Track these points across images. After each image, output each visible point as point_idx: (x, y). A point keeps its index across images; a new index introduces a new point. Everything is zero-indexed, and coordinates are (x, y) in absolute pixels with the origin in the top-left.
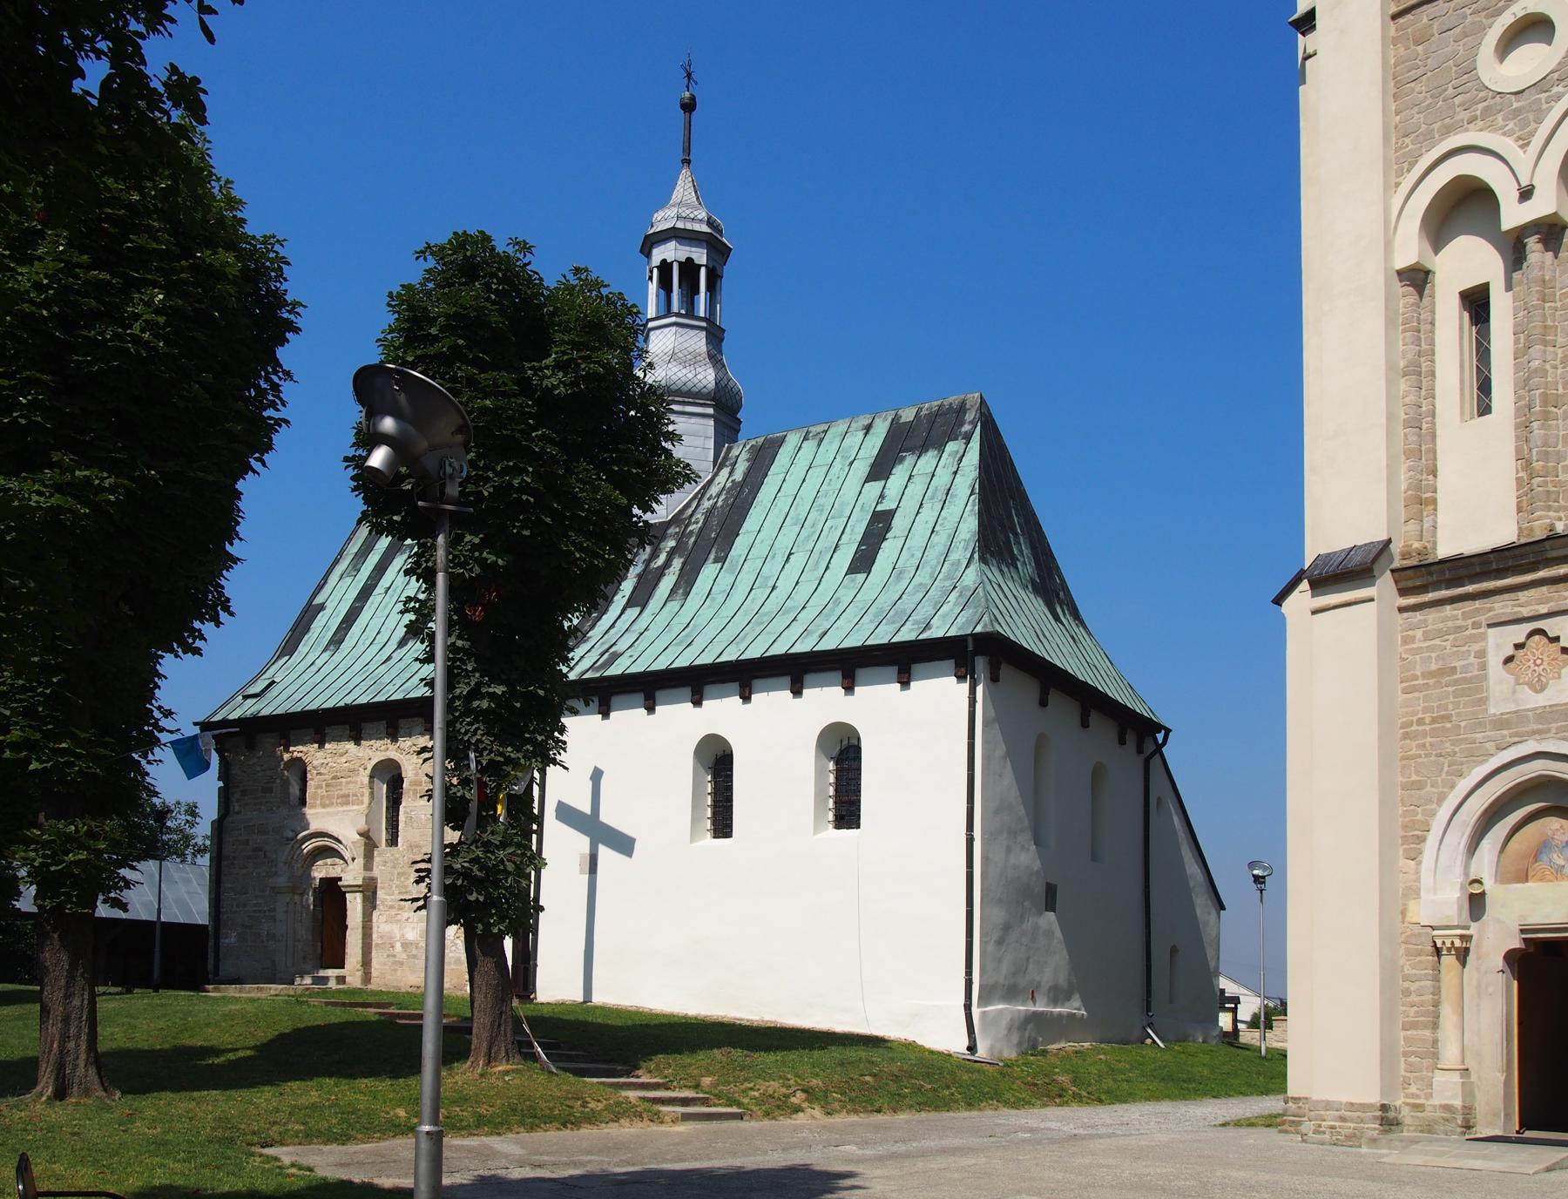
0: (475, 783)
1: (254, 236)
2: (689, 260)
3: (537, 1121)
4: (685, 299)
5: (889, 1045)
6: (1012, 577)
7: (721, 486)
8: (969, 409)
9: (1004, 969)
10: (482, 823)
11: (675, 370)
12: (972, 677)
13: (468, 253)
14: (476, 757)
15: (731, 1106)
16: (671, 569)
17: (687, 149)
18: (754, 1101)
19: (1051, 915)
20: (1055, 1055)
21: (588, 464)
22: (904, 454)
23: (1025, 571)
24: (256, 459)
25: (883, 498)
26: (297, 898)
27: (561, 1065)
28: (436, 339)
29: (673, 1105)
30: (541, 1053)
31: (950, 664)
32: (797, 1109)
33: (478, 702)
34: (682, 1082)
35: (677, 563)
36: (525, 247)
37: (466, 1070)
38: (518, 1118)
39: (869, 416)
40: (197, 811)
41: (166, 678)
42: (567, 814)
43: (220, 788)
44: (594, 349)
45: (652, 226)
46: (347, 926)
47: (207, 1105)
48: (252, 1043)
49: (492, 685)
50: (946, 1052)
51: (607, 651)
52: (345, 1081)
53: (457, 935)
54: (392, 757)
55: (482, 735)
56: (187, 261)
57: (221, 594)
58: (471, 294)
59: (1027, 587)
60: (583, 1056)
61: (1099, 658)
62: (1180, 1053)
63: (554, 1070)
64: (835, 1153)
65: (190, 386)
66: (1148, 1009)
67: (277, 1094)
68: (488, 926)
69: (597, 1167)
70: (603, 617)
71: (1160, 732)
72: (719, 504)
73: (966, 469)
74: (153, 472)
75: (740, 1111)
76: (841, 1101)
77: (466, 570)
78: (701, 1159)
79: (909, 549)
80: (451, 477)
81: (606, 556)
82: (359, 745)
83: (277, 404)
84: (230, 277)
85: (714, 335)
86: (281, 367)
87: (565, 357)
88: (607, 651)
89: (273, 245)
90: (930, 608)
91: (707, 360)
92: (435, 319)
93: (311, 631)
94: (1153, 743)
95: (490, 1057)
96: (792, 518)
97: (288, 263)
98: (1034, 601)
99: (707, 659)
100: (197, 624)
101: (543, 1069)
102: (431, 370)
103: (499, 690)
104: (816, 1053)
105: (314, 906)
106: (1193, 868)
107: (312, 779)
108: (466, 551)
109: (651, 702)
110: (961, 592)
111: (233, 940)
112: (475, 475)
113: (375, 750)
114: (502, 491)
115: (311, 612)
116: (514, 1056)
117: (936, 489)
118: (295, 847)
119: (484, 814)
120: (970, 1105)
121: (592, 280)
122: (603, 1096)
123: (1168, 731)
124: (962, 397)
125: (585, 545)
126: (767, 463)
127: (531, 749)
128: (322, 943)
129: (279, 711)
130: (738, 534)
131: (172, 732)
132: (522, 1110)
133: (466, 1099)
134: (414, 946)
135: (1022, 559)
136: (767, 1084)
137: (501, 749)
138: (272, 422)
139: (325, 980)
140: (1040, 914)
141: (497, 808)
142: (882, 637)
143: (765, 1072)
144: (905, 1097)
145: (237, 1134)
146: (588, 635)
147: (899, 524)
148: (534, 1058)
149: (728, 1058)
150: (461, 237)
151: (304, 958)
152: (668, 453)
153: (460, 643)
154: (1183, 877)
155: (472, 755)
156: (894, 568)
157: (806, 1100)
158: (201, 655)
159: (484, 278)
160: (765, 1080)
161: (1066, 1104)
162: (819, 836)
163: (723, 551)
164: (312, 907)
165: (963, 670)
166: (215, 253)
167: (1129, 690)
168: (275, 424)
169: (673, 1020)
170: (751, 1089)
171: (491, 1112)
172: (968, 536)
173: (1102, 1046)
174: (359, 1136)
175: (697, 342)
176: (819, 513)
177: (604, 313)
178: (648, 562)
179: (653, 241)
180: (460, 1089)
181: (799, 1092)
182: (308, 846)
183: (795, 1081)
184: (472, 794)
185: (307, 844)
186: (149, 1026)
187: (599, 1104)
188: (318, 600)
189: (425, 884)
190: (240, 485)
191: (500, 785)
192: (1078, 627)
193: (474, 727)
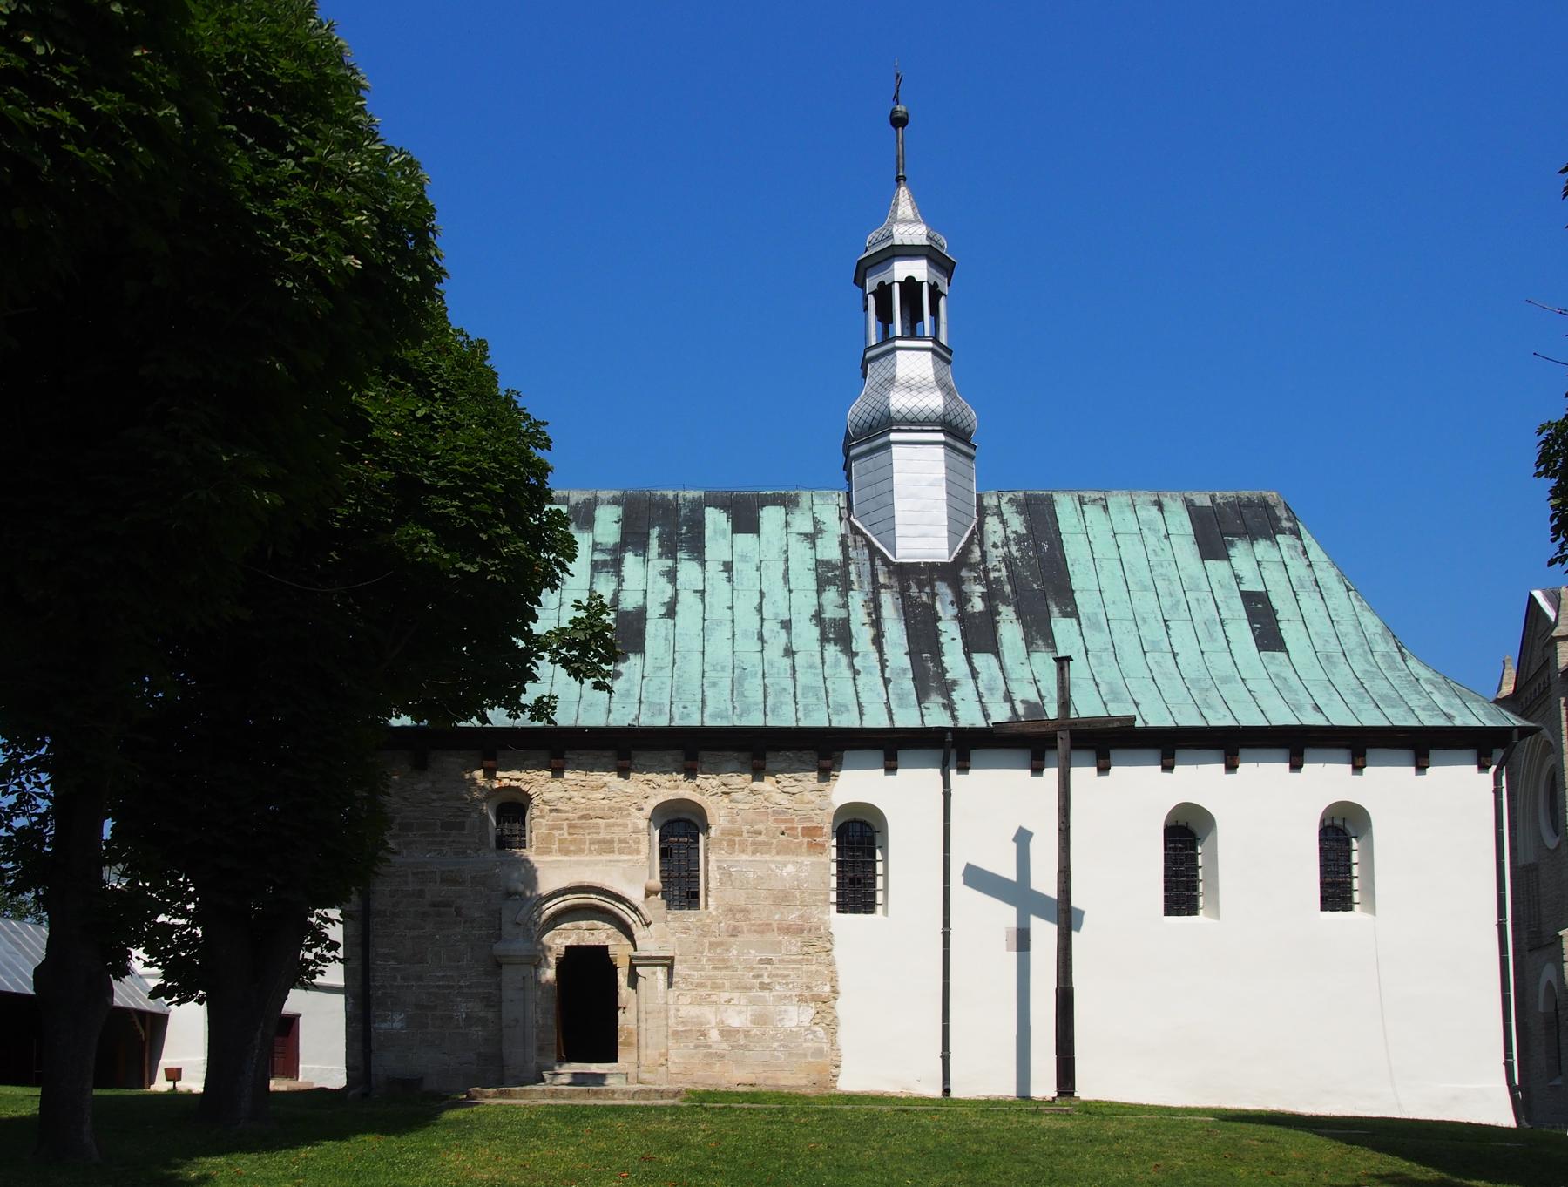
53: (815, 1021)
82: (627, 778)
111: (397, 1025)
113: (668, 787)
182: (550, 908)
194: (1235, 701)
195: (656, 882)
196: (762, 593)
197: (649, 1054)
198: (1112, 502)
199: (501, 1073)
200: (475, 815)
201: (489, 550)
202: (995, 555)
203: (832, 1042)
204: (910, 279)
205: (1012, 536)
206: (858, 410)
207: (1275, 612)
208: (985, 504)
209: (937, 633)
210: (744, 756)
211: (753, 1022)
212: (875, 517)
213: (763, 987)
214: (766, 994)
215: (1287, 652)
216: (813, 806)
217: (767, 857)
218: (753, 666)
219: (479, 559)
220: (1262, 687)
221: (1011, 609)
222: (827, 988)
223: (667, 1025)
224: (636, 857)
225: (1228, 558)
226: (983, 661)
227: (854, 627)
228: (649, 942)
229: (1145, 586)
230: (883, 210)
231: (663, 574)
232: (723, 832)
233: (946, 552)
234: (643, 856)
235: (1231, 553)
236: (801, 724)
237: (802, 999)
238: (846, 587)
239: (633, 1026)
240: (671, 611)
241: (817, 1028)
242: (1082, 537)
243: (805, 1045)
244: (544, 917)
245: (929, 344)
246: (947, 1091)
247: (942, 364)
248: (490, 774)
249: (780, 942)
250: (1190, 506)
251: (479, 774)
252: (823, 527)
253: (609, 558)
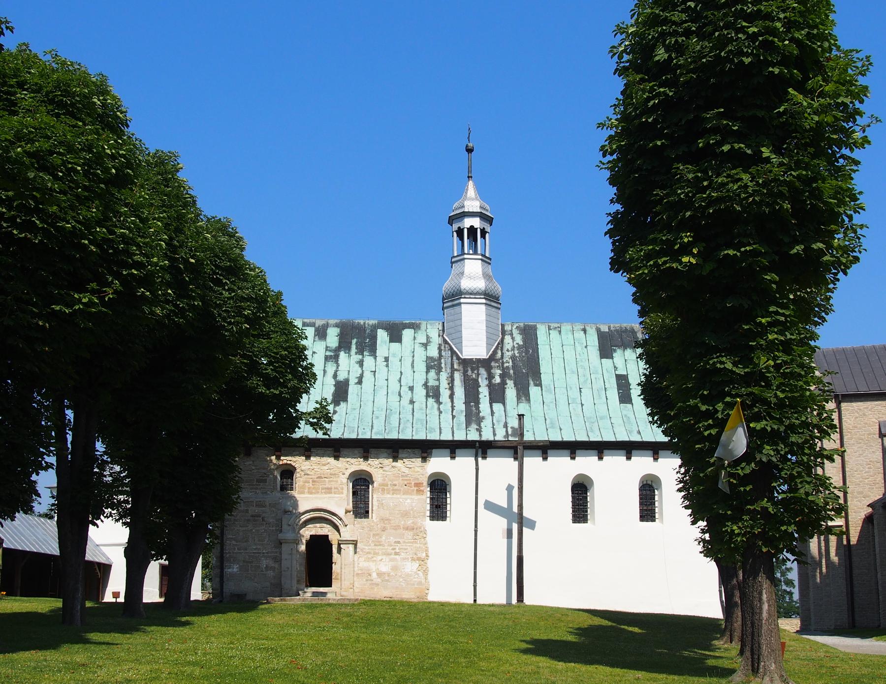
17: (469, 171)
82: (338, 460)
111: (235, 570)
113: (355, 464)
194: (604, 428)
195: (350, 507)
196: (401, 372)
197: (346, 584)
198: (563, 328)
199: (280, 590)
200: (271, 476)
201: (284, 385)
202: (507, 355)
203: (426, 579)
204: (472, 227)
205: (516, 346)
206: (447, 286)
207: (630, 385)
208: (505, 329)
209: (478, 393)
210: (390, 451)
211: (392, 569)
212: (454, 336)
213: (396, 554)
214: (397, 557)
215: (632, 404)
216: (419, 473)
217: (399, 496)
218: (395, 409)
219: (279, 389)
220: (617, 421)
221: (512, 382)
222: (424, 555)
223: (354, 571)
224: (342, 495)
225: (612, 358)
226: (497, 407)
227: (441, 390)
228: (347, 533)
229: (573, 371)
230: (461, 192)
231: (357, 362)
232: (380, 485)
233: (485, 354)
234: (344, 495)
235: (614, 355)
236: (413, 438)
237: (413, 559)
238: (439, 370)
239: (339, 571)
240: (360, 382)
241: (419, 572)
242: (548, 347)
243: (414, 580)
244: (301, 522)
245: (480, 257)
246: (475, 601)
247: (486, 265)
248: (278, 458)
249: (404, 534)
250: (598, 330)
251: (273, 458)
252: (431, 340)
253: (333, 354)
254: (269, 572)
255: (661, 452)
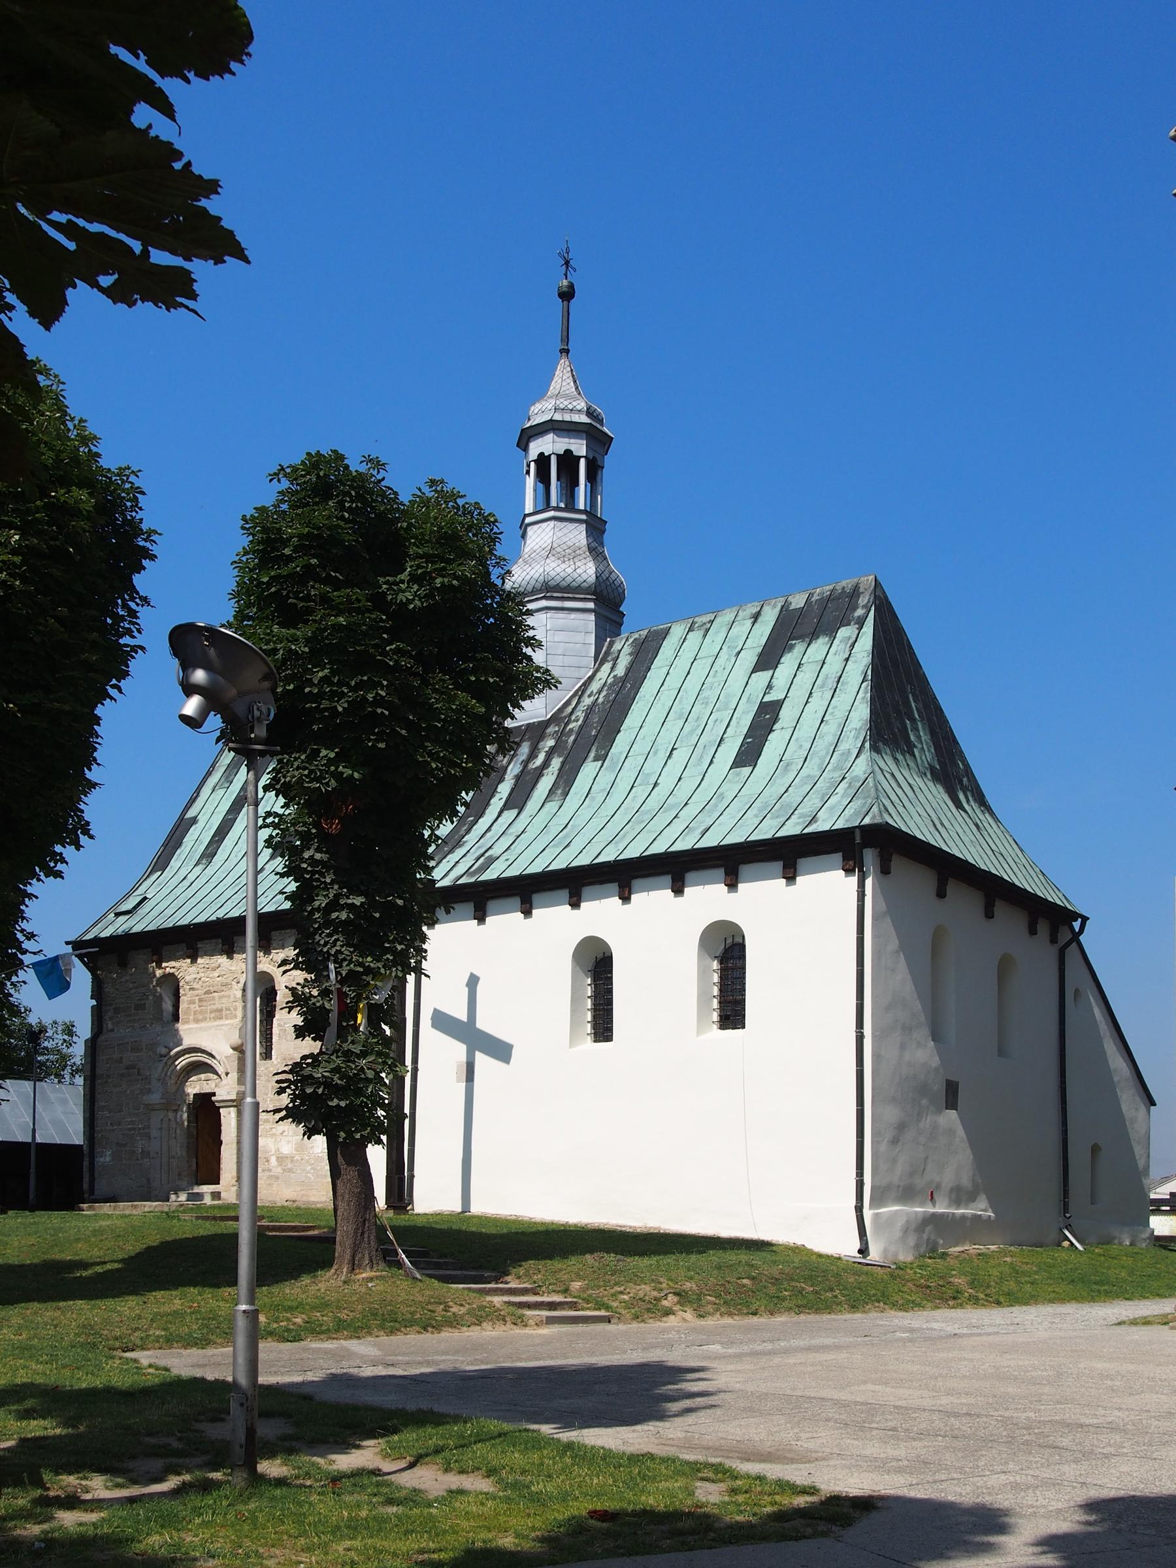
0: (335, 994)
1: (109, 469)
2: (568, 452)
3: (397, 1325)
4: (564, 492)
5: (774, 1248)
6: (908, 765)
7: (603, 681)
8: (863, 593)
9: (899, 1169)
10: (342, 1034)
11: (553, 565)
12: (861, 870)
13: (322, 473)
14: (336, 968)
15: (599, 1309)
16: (550, 769)
17: (566, 338)
18: (623, 1304)
19: (953, 1114)
20: (957, 1257)
21: (444, 675)
22: (794, 642)
23: (924, 757)
24: (113, 686)
25: (771, 689)
26: (171, 1115)
27: (424, 1272)
28: (289, 559)
29: (540, 1310)
30: (406, 1260)
31: (838, 857)
32: (668, 1312)
33: (337, 914)
34: (550, 1287)
35: (556, 763)
36: (378, 464)
37: (329, 1278)
38: (379, 1322)
39: (757, 604)
40: (74, 1029)
41: (37, 897)
42: (442, 1022)
43: (93, 1007)
44: (449, 562)
45: (529, 419)
46: (221, 1142)
47: (72, 1313)
48: (120, 1257)
49: (351, 897)
50: (835, 1255)
51: (483, 855)
52: (207, 1290)
54: (265, 969)
55: (342, 946)
56: (42, 501)
57: (81, 818)
58: (325, 513)
59: (925, 774)
60: (452, 1263)
61: (1006, 844)
62: (1100, 1255)
63: (418, 1276)
64: (697, 1351)
65: (47, 621)
66: (1066, 1210)
67: (141, 1303)
68: (350, 1134)
69: (451, 1366)
70: (480, 821)
71: (1076, 920)
72: (601, 700)
73: (858, 655)
74: (11, 705)
75: (607, 1314)
76: (715, 1304)
77: (322, 784)
78: (557, 1358)
79: (797, 740)
80: (259, 720)
81: (464, 765)
82: (232, 959)
83: (133, 632)
84: (84, 512)
85: (595, 528)
86: (138, 593)
87: (420, 571)
88: (483, 855)
89: (128, 477)
90: (817, 801)
91: (588, 553)
92: (289, 540)
93: (184, 845)
94: (1069, 932)
95: (354, 1264)
96: (676, 712)
97: (143, 493)
98: (933, 788)
99: (584, 860)
100: (58, 848)
101: (407, 1275)
102: (285, 589)
103: (358, 901)
104: (693, 1257)
105: (188, 1122)
106: (1117, 1062)
107: (185, 995)
108: (322, 766)
109: (528, 905)
110: (850, 783)
112: (329, 692)
114: (357, 706)
115: (183, 825)
116: (378, 1263)
117: (827, 677)
118: (169, 1063)
119: (345, 1024)
120: (853, 1307)
121: (447, 492)
122: (466, 1300)
123: (1085, 919)
124: (856, 580)
125: (442, 755)
126: (650, 656)
127: (391, 958)
128: (197, 1159)
129: (150, 928)
130: (619, 731)
131: (34, 953)
132: (383, 1315)
133: (326, 1305)
134: (289, 1160)
135: (919, 746)
136: (638, 1287)
137: (361, 960)
138: (129, 649)
139: (200, 1196)
140: (939, 1112)
141: (357, 1017)
142: (766, 832)
143: (637, 1276)
144: (784, 1299)
145: (100, 1339)
146: (464, 840)
147: (787, 715)
148: (399, 1265)
149: (599, 1263)
150: (313, 457)
151: (179, 1175)
152: (529, 659)
153: (318, 856)
154: (1108, 1073)
155: (332, 966)
156: (781, 761)
157: (679, 1303)
158: (63, 878)
159: (337, 496)
160: (635, 1284)
161: (961, 1306)
162: (701, 1038)
163: (603, 748)
164: (186, 1123)
165: (851, 863)
166: (69, 491)
167: (1041, 877)
168: (131, 651)
169: (551, 1228)
170: (621, 1293)
171: (352, 1317)
172: (858, 725)
173: (1012, 1248)
174: (219, 1341)
175: (577, 535)
176: (704, 706)
177: (460, 523)
178: (526, 763)
179: (530, 435)
180: (322, 1295)
181: (670, 1295)
182: (181, 1063)
183: (668, 1284)
184: (332, 1005)
185: (180, 1060)
186: (20, 1242)
187: (462, 1308)
188: (191, 814)
189: (287, 1094)
190: (99, 711)
191: (361, 994)
192: (984, 813)
193: (333, 939)
254: (145, 1160)
255: (536, 898)
